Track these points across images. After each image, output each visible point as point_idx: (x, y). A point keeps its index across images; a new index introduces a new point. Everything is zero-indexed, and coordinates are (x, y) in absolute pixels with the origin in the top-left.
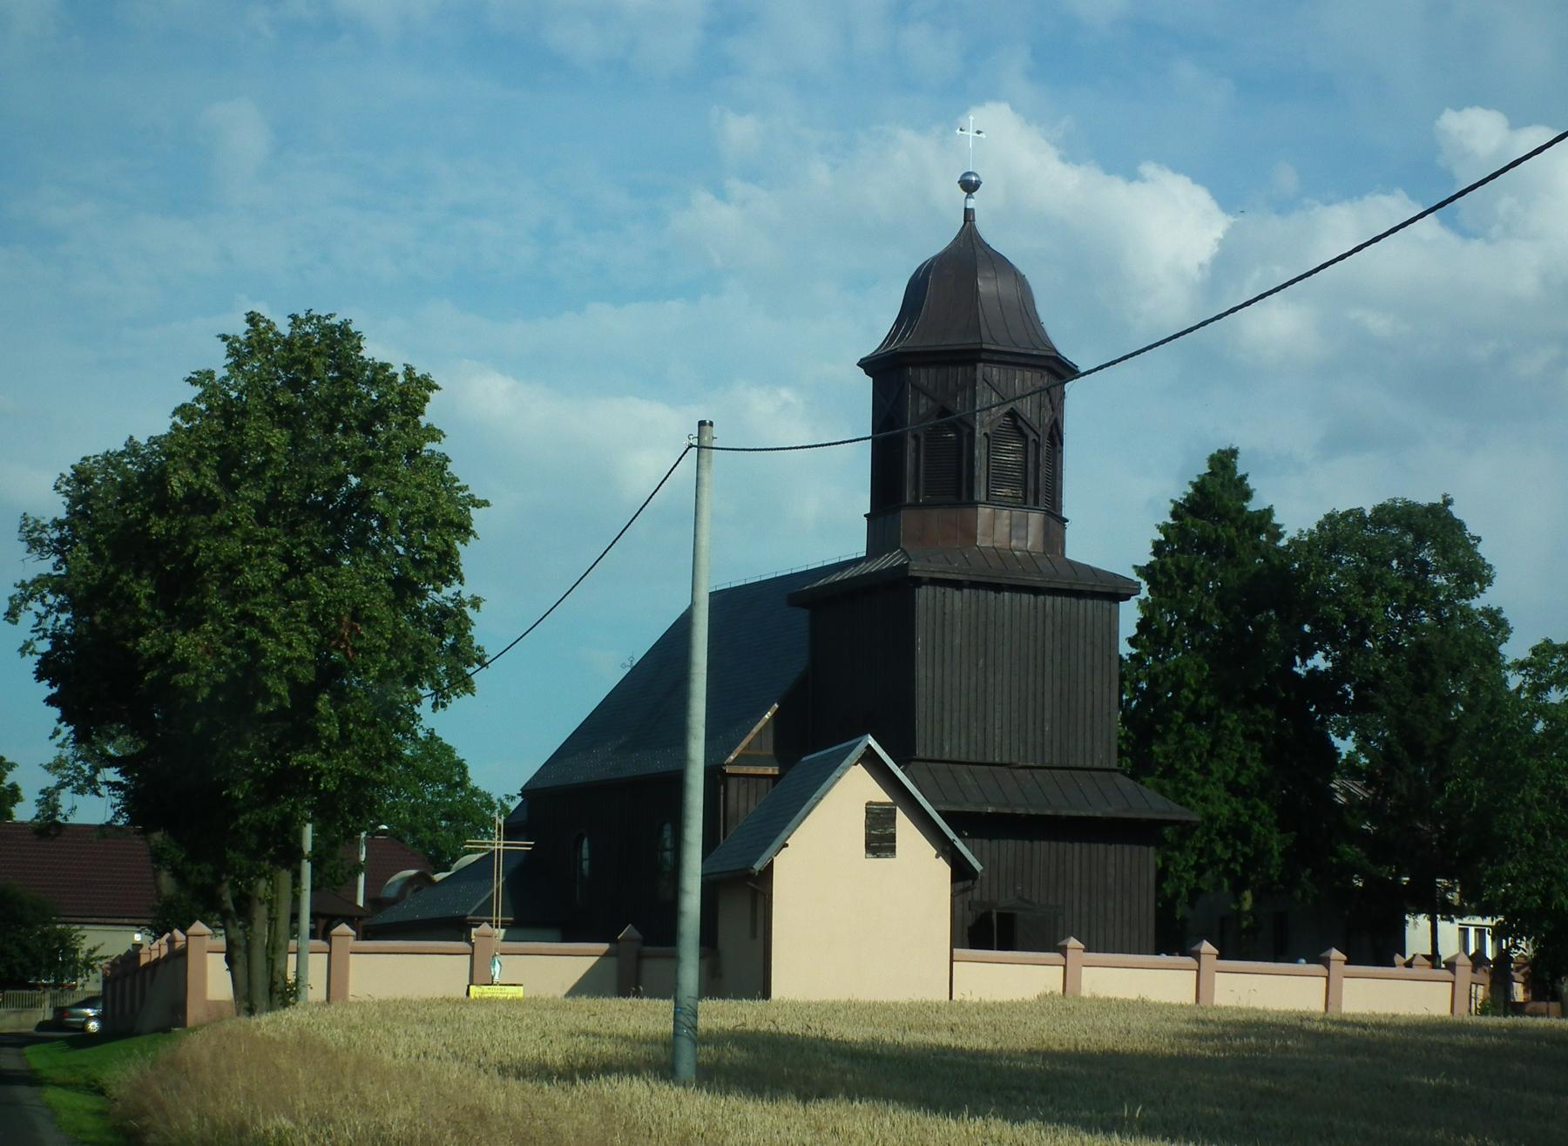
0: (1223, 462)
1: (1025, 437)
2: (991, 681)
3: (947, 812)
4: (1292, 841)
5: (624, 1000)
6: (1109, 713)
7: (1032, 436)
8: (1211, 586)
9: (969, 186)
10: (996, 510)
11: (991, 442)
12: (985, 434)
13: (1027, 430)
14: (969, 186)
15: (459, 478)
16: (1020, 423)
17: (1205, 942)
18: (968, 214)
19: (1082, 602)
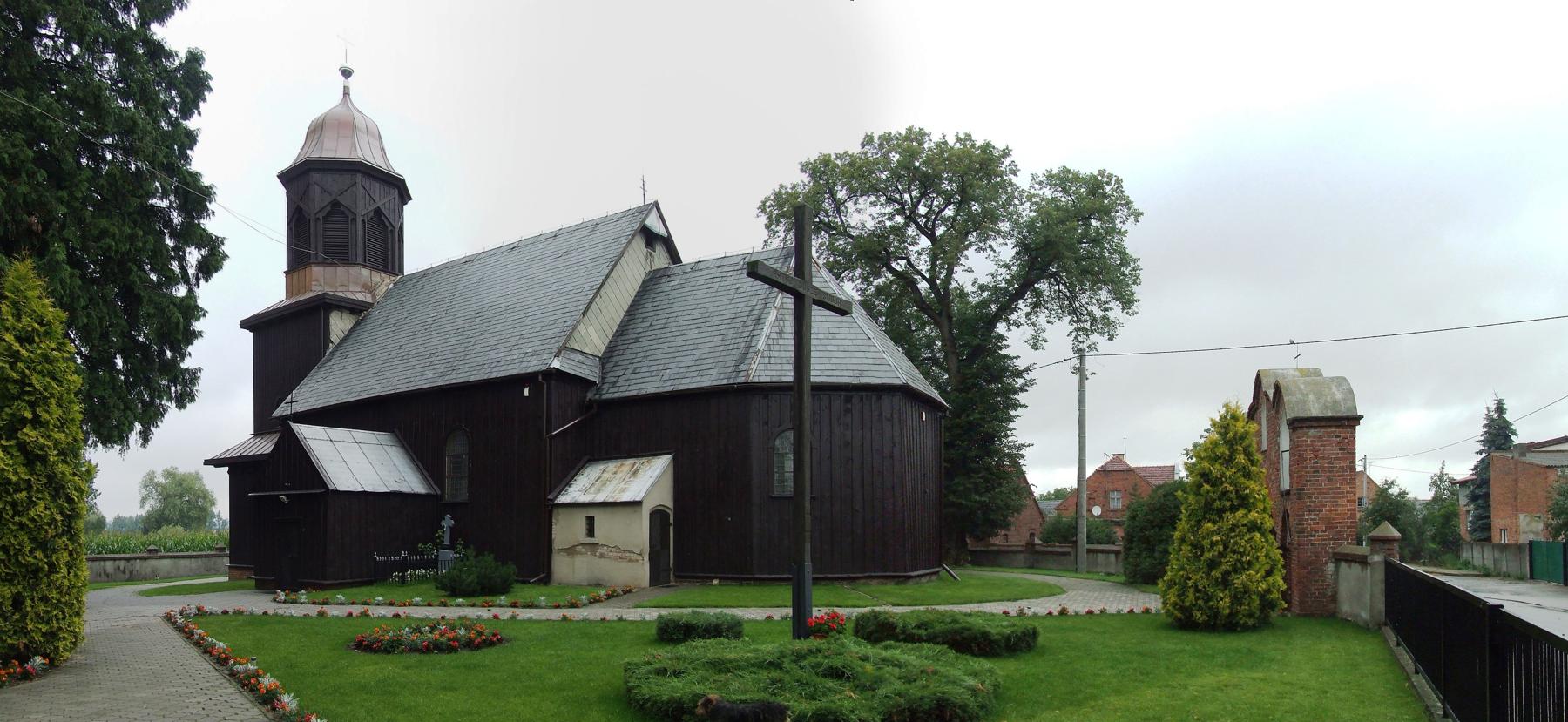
7: (390, 228)
9: (346, 73)
13: (347, 212)
14: (346, 73)
16: (383, 218)
18: (346, 93)
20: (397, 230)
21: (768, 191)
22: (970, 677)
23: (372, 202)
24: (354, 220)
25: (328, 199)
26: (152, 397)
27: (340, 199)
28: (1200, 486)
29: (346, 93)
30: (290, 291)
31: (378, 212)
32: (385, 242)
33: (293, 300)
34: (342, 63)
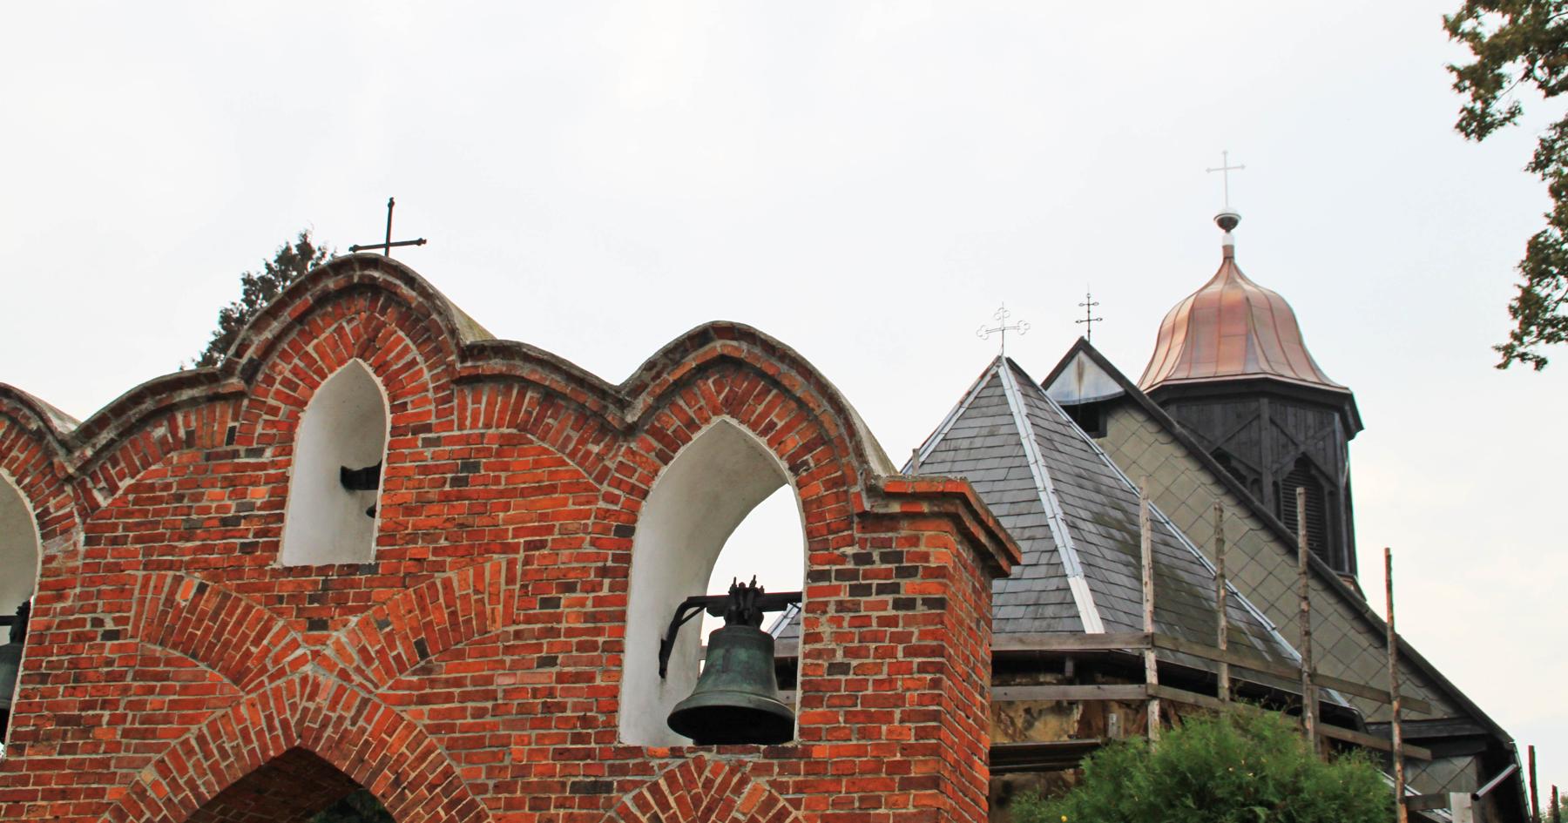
7: (1327, 488)
9: (1227, 223)
13: (1323, 482)
14: (1227, 223)
34: (1232, 208)
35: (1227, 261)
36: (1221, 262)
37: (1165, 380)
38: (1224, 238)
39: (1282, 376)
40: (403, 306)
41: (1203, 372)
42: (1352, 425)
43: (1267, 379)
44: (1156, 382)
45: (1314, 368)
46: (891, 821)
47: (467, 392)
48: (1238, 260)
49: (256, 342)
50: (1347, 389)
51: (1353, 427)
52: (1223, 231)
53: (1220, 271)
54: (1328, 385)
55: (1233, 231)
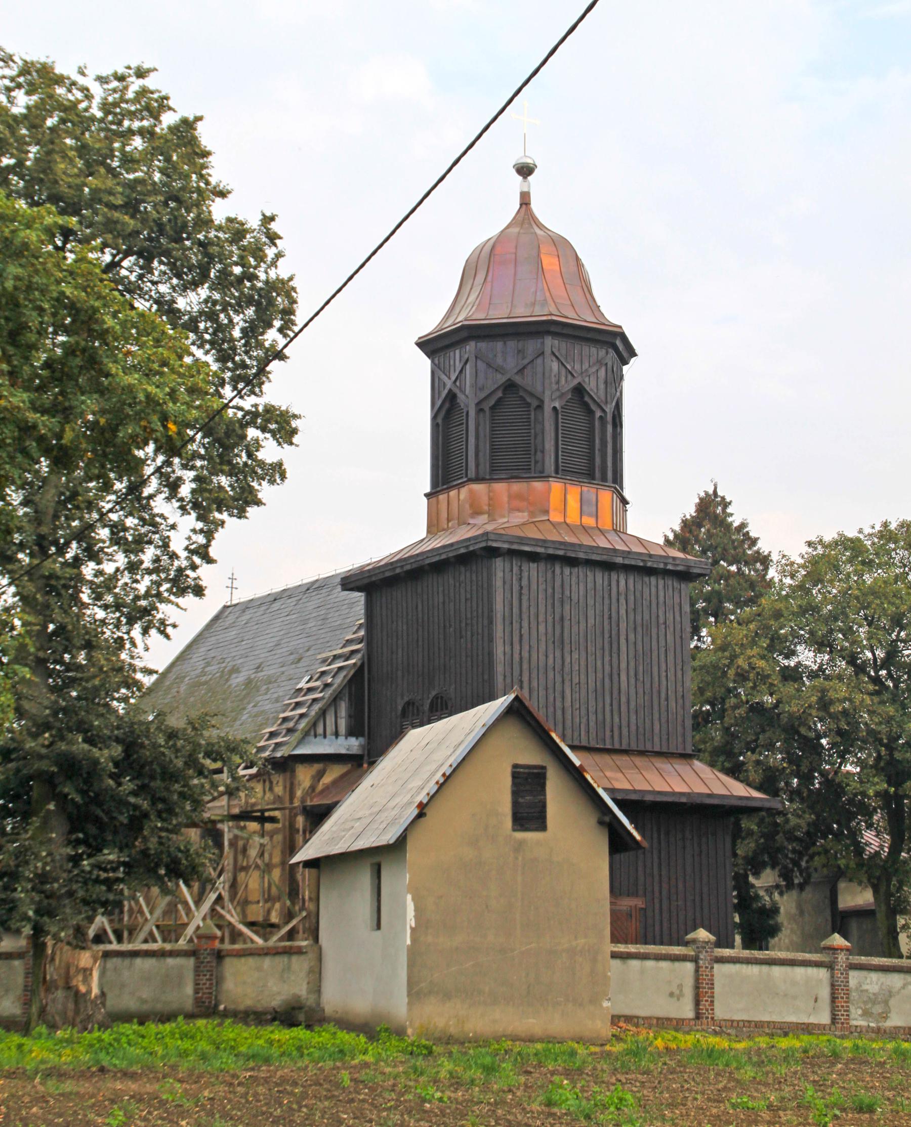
0: (288, 358)
1: (591, 412)
2: (568, 660)
3: (622, 800)
4: (743, 825)
5: (283, 997)
6: (683, 696)
7: (598, 414)
8: (64, 479)
9: (525, 171)
10: (568, 486)
11: (560, 416)
12: (555, 408)
13: (593, 407)
14: (525, 171)
15: (286, 481)
16: (587, 399)
17: (836, 935)
18: (525, 200)
19: (614, 576)
20: (609, 418)
21: (514, 163)
22: (12, 747)
23: (570, 377)
24: (540, 407)
25: (501, 379)
26: (80, 610)
27: (518, 379)
28: (250, 455)
29: (525, 200)
30: (433, 526)
31: (579, 391)
32: (591, 441)
33: (437, 543)
34: (518, 157)
35: (524, 206)
36: (518, 206)
37: (466, 320)
38: (521, 185)
39: (567, 318)
40: (279, 1121)
41: (499, 314)
42: (626, 352)
43: (463, 326)
44: (458, 320)
45: (595, 308)
46: (906, 1045)
47: (588, 573)
48: (534, 206)
49: (106, 752)
50: (620, 327)
51: (625, 354)
52: (521, 178)
53: (519, 211)
54: (604, 324)
55: (529, 178)
